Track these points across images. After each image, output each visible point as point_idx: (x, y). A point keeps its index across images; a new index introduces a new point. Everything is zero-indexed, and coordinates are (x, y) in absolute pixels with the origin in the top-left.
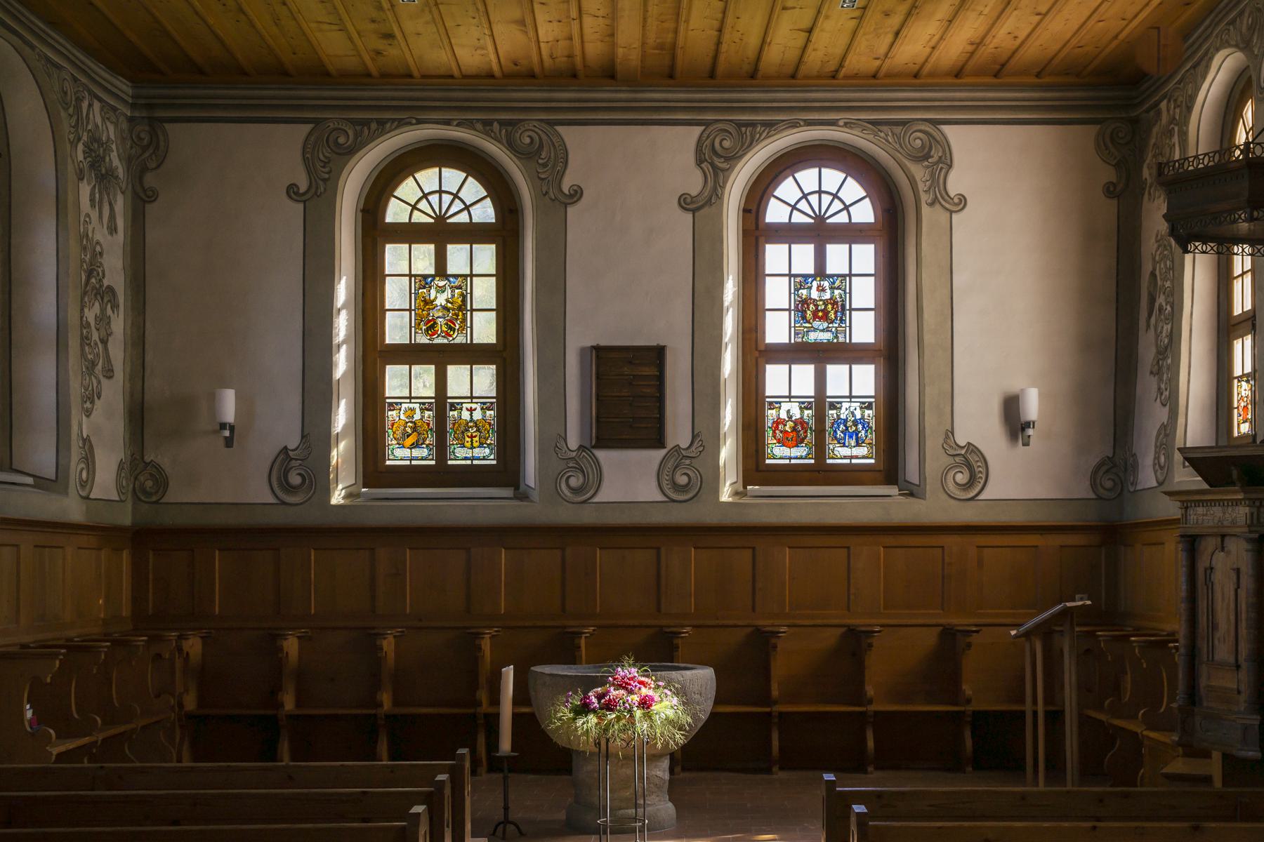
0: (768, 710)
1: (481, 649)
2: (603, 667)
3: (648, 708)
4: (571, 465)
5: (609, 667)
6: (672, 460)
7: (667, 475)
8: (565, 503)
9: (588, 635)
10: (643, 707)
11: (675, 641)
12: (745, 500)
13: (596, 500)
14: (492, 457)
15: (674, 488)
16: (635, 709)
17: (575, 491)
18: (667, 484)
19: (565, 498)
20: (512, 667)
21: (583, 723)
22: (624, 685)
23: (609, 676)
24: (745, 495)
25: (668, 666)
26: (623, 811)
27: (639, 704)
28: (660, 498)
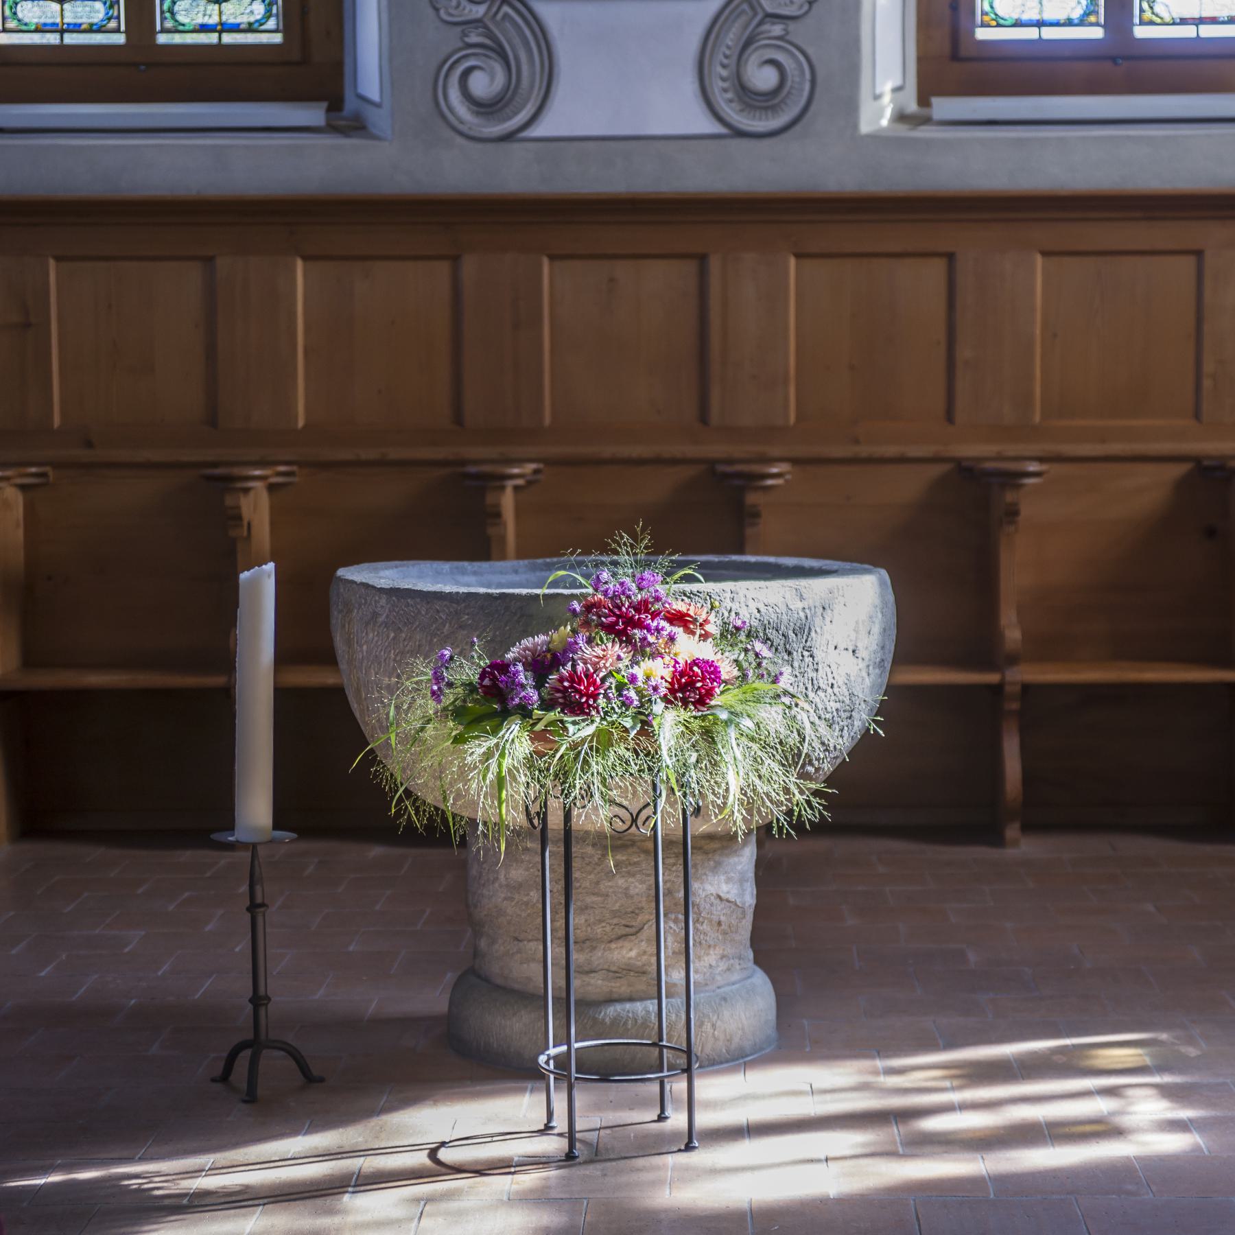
0: (992, 678)
1: (239, 518)
2: (550, 568)
3: (701, 702)
4: (474, 39)
5: (572, 568)
6: (737, 25)
7: (724, 66)
8: (459, 140)
9: (520, 482)
10: (685, 703)
11: (752, 498)
12: (924, 132)
13: (539, 131)
14: (271, 24)
15: (740, 100)
16: (658, 707)
17: (488, 108)
18: (725, 90)
19: (460, 127)
20: (270, 567)
21: (488, 755)
22: (621, 626)
23: (573, 596)
24: (927, 120)
25: (747, 563)
26: (619, 1007)
27: (672, 691)
28: (707, 126)
